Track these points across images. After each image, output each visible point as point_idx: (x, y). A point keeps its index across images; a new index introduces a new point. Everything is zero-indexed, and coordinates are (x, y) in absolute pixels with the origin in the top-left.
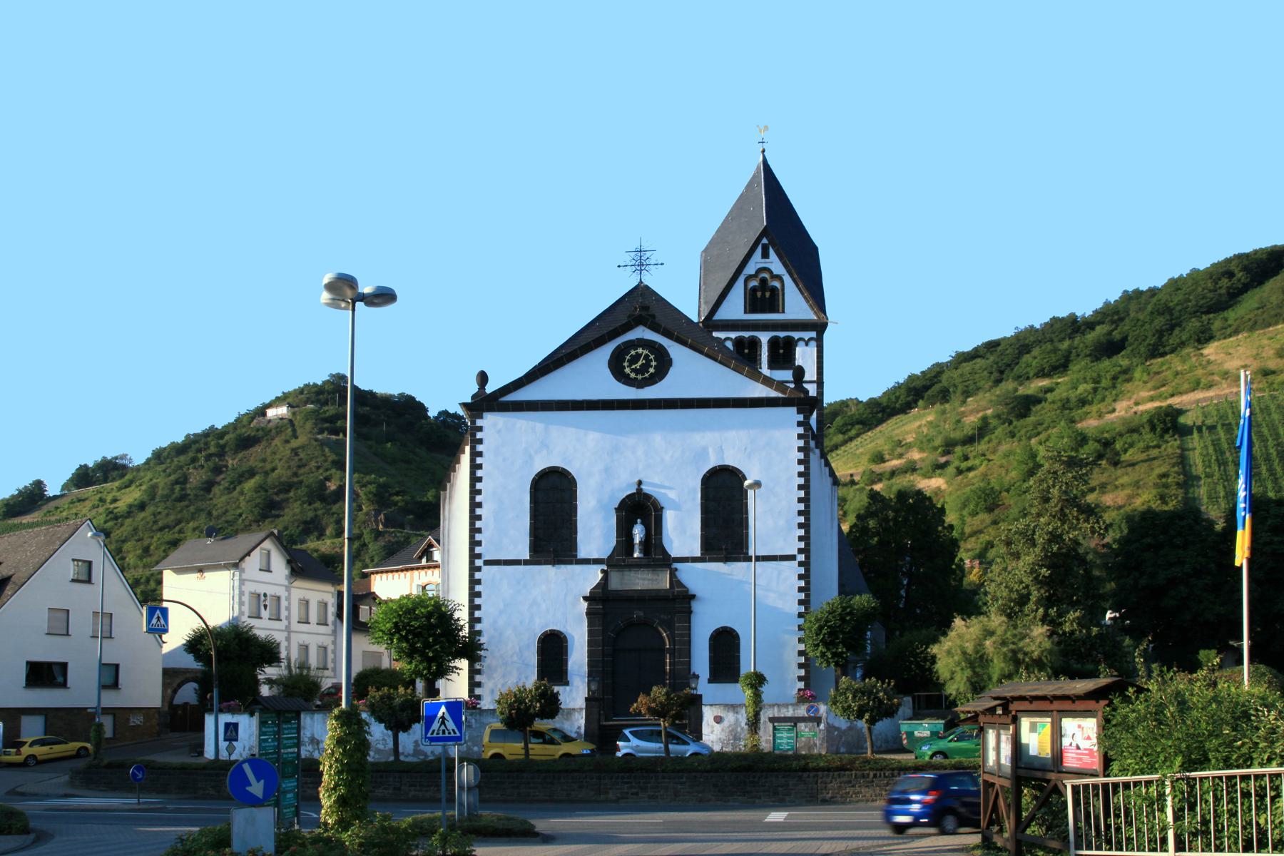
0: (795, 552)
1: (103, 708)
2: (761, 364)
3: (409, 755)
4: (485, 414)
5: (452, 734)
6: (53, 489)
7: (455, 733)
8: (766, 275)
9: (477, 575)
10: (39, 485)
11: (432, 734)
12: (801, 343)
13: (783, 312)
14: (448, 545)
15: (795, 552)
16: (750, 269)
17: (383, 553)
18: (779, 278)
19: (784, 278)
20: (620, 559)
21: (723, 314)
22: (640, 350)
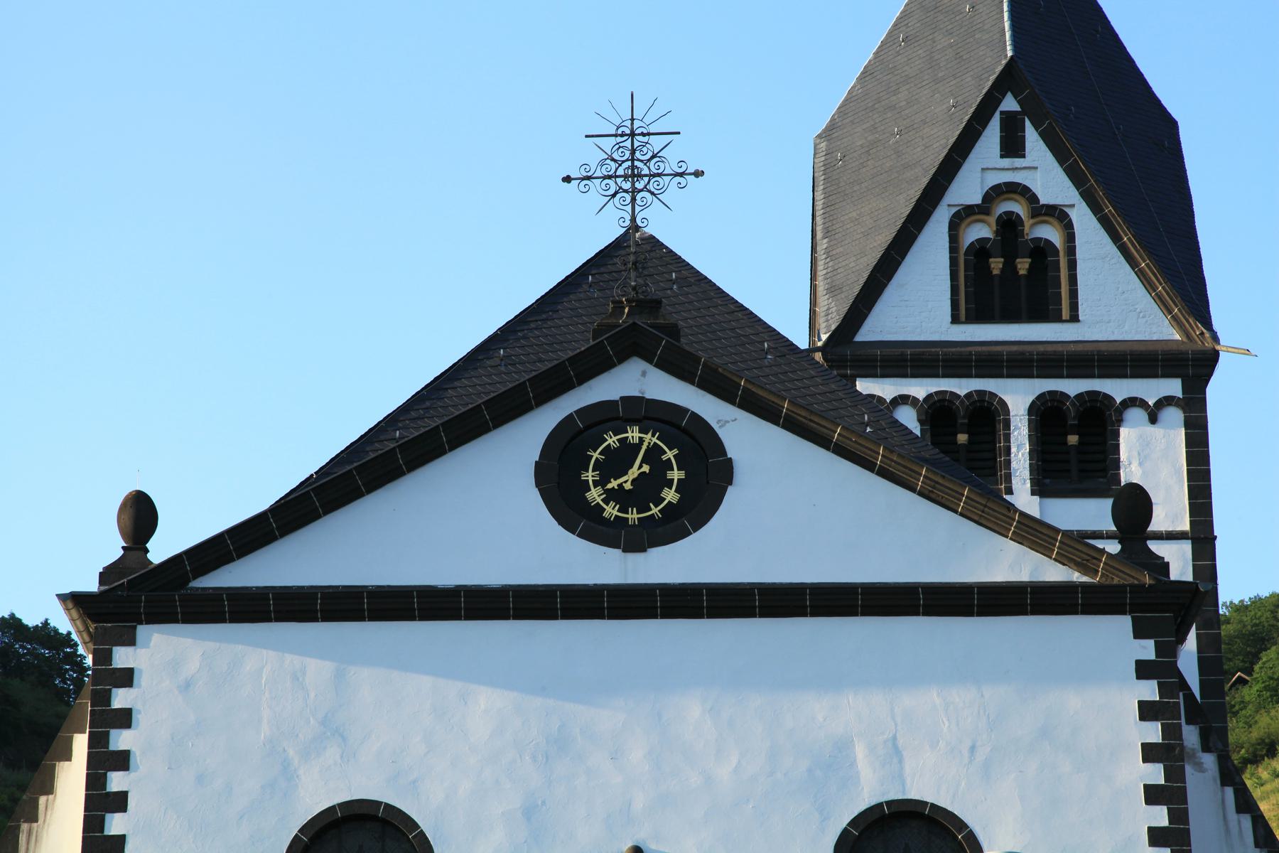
2: (1008, 478)
8: (1017, 207)
12: (1135, 416)
13: (1074, 318)
18: (1058, 214)
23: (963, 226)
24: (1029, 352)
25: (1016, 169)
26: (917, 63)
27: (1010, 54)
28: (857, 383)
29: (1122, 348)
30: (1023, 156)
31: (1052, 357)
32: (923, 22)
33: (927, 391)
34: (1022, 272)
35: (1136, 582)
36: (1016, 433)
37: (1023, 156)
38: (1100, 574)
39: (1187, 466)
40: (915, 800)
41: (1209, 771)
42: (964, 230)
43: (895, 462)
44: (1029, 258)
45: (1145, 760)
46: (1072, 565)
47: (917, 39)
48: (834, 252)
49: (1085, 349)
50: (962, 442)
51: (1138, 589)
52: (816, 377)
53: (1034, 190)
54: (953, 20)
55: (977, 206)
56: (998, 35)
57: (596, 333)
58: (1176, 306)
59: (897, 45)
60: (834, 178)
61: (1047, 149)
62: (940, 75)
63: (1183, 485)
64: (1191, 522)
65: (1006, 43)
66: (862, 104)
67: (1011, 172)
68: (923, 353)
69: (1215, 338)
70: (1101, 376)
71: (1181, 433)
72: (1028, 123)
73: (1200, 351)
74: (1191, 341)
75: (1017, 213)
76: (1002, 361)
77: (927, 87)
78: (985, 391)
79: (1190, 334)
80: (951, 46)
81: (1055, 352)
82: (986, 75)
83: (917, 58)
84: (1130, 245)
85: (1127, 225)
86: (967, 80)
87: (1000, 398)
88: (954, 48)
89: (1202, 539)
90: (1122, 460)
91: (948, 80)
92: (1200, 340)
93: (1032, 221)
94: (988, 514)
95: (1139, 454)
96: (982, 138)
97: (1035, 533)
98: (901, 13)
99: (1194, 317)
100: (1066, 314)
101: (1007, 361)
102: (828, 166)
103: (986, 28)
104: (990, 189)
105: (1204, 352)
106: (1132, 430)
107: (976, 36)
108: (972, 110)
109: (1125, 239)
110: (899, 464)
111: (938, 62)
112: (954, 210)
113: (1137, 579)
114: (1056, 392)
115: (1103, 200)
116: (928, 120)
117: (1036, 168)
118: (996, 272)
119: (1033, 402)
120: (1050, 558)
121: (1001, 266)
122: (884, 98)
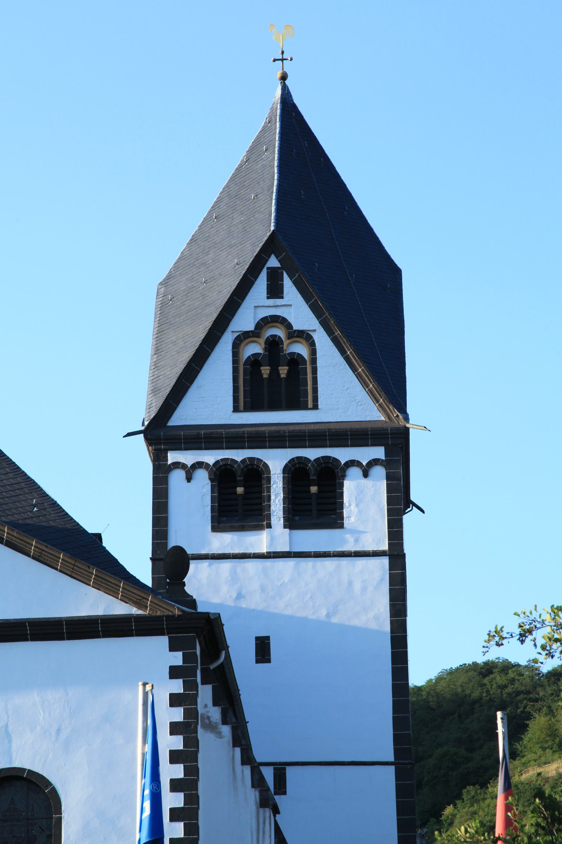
2: (269, 517)
8: (279, 332)
12: (354, 472)
13: (315, 407)
17: (545, 727)
19: (315, 336)
23: (242, 345)
24: (282, 431)
25: (278, 306)
26: (221, 234)
27: (272, 228)
28: (168, 454)
29: (343, 426)
30: (282, 298)
31: (298, 434)
32: (228, 205)
33: (215, 458)
34: (283, 376)
35: (171, 614)
36: (274, 486)
37: (282, 298)
38: (148, 608)
39: (387, 506)
40: (18, 768)
41: (226, 737)
42: (244, 348)
43: (15, 537)
44: (287, 366)
45: (172, 733)
46: (131, 603)
47: (224, 217)
48: (159, 364)
49: (321, 428)
50: (240, 493)
51: (171, 618)
52: (10, 473)
53: (289, 320)
54: (245, 205)
55: (251, 331)
56: (268, 215)
58: (381, 398)
59: (212, 221)
60: (166, 312)
61: (298, 293)
62: (233, 242)
63: (384, 519)
64: (389, 544)
65: (271, 221)
66: (188, 261)
67: (274, 308)
68: (212, 433)
69: (407, 419)
70: (331, 446)
71: (383, 485)
72: (285, 275)
73: (397, 428)
74: (391, 421)
75: (279, 336)
76: (266, 437)
77: (225, 250)
78: (254, 458)
79: (391, 417)
80: (241, 222)
81: (300, 430)
82: (257, 243)
83: (221, 230)
84: (351, 357)
85: (349, 343)
86: (247, 246)
87: (265, 463)
88: (243, 224)
89: (396, 555)
90: (344, 502)
91: (237, 246)
92: (396, 420)
93: (288, 341)
94: (76, 570)
95: (356, 499)
96: (255, 286)
97: (106, 582)
98: (217, 199)
99: (392, 404)
100: (310, 404)
101: (269, 437)
102: (163, 304)
103: (262, 210)
104: (260, 320)
105: (398, 429)
106: (351, 482)
107: (256, 216)
108: (247, 267)
109: (349, 353)
110: (18, 538)
111: (233, 233)
112: (236, 335)
113: (172, 612)
114: (302, 457)
115: (334, 327)
116: (222, 273)
117: (291, 305)
118: (265, 376)
119: (286, 465)
120: (118, 598)
121: (268, 372)
122: (201, 257)
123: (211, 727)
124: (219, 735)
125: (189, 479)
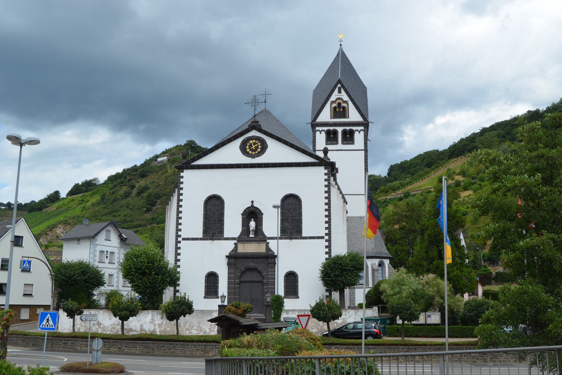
0: (324, 235)
1: (10, 305)
3: (138, 331)
4: (185, 171)
5: (51, 327)
6: (63, 195)
7: (52, 326)
9: (179, 245)
10: (57, 193)
11: (42, 326)
13: (348, 118)
14: (169, 230)
15: (324, 235)
16: (333, 98)
18: (346, 102)
20: (244, 237)
21: (320, 119)
22: (251, 142)
57: (248, 126)
123: (333, 186)
124: (335, 187)
125: (320, 133)
